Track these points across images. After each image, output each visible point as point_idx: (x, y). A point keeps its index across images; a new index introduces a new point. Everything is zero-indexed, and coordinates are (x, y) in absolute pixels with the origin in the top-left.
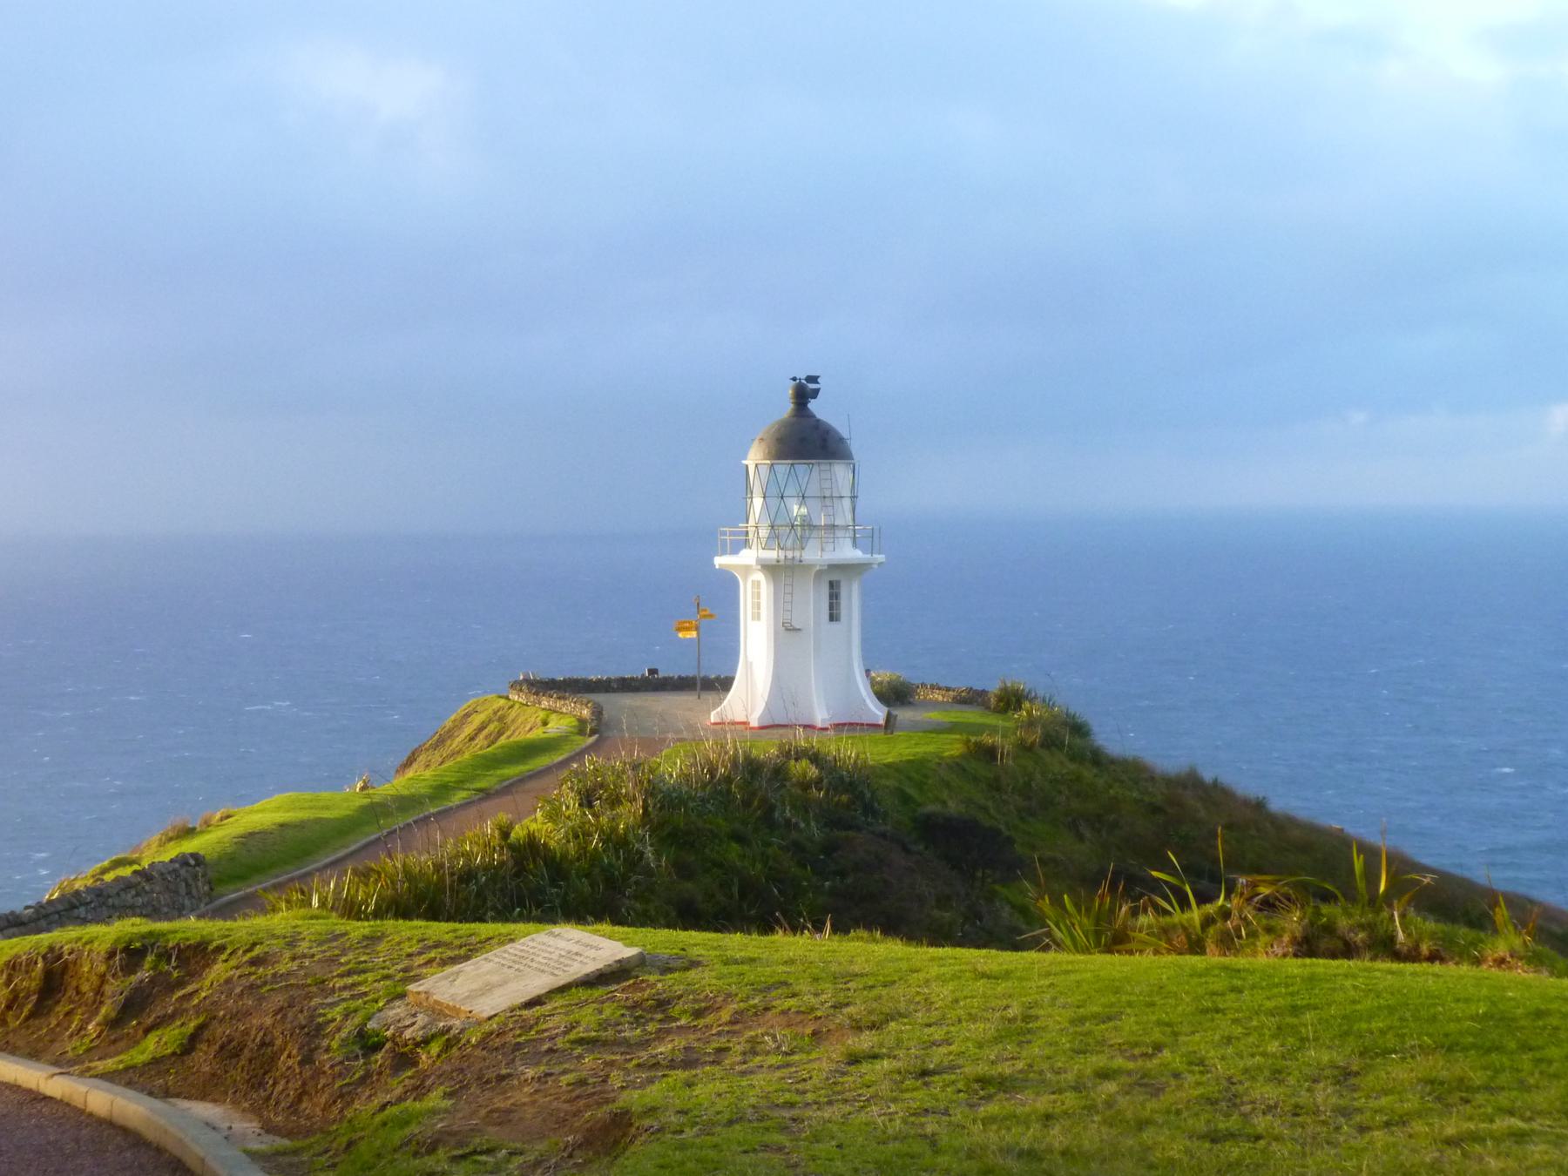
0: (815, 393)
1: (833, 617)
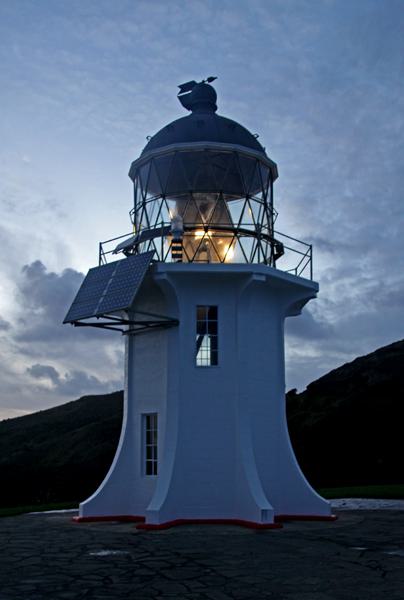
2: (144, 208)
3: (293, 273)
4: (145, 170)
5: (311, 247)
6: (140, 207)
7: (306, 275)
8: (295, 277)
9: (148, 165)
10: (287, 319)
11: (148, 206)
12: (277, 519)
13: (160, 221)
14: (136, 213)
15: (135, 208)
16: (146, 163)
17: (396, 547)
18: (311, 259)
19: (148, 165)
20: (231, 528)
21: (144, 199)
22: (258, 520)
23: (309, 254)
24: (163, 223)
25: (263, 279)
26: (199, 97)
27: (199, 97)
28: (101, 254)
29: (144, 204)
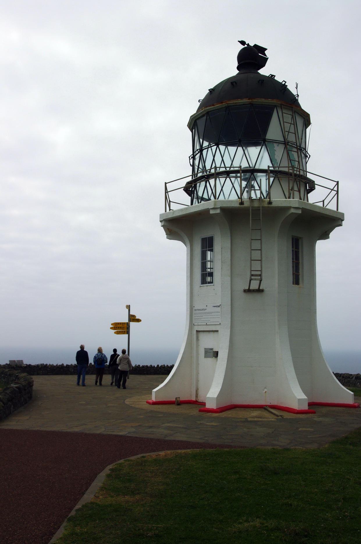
0: (263, 62)
1: (296, 281)
2: (202, 154)
3: (321, 204)
4: (201, 123)
5: (338, 182)
6: (197, 153)
7: (332, 206)
8: (323, 208)
9: (205, 118)
10: (318, 242)
11: (204, 152)
12: (310, 404)
13: (213, 166)
14: (194, 158)
15: (193, 154)
16: (203, 116)
17: (249, 419)
18: (337, 191)
19: (205, 118)
20: (334, 408)
21: (201, 146)
22: (295, 406)
23: (336, 189)
24: (216, 168)
25: (300, 212)
26: (252, 57)
27: (252, 57)
28: (168, 202)
29: (201, 150)
